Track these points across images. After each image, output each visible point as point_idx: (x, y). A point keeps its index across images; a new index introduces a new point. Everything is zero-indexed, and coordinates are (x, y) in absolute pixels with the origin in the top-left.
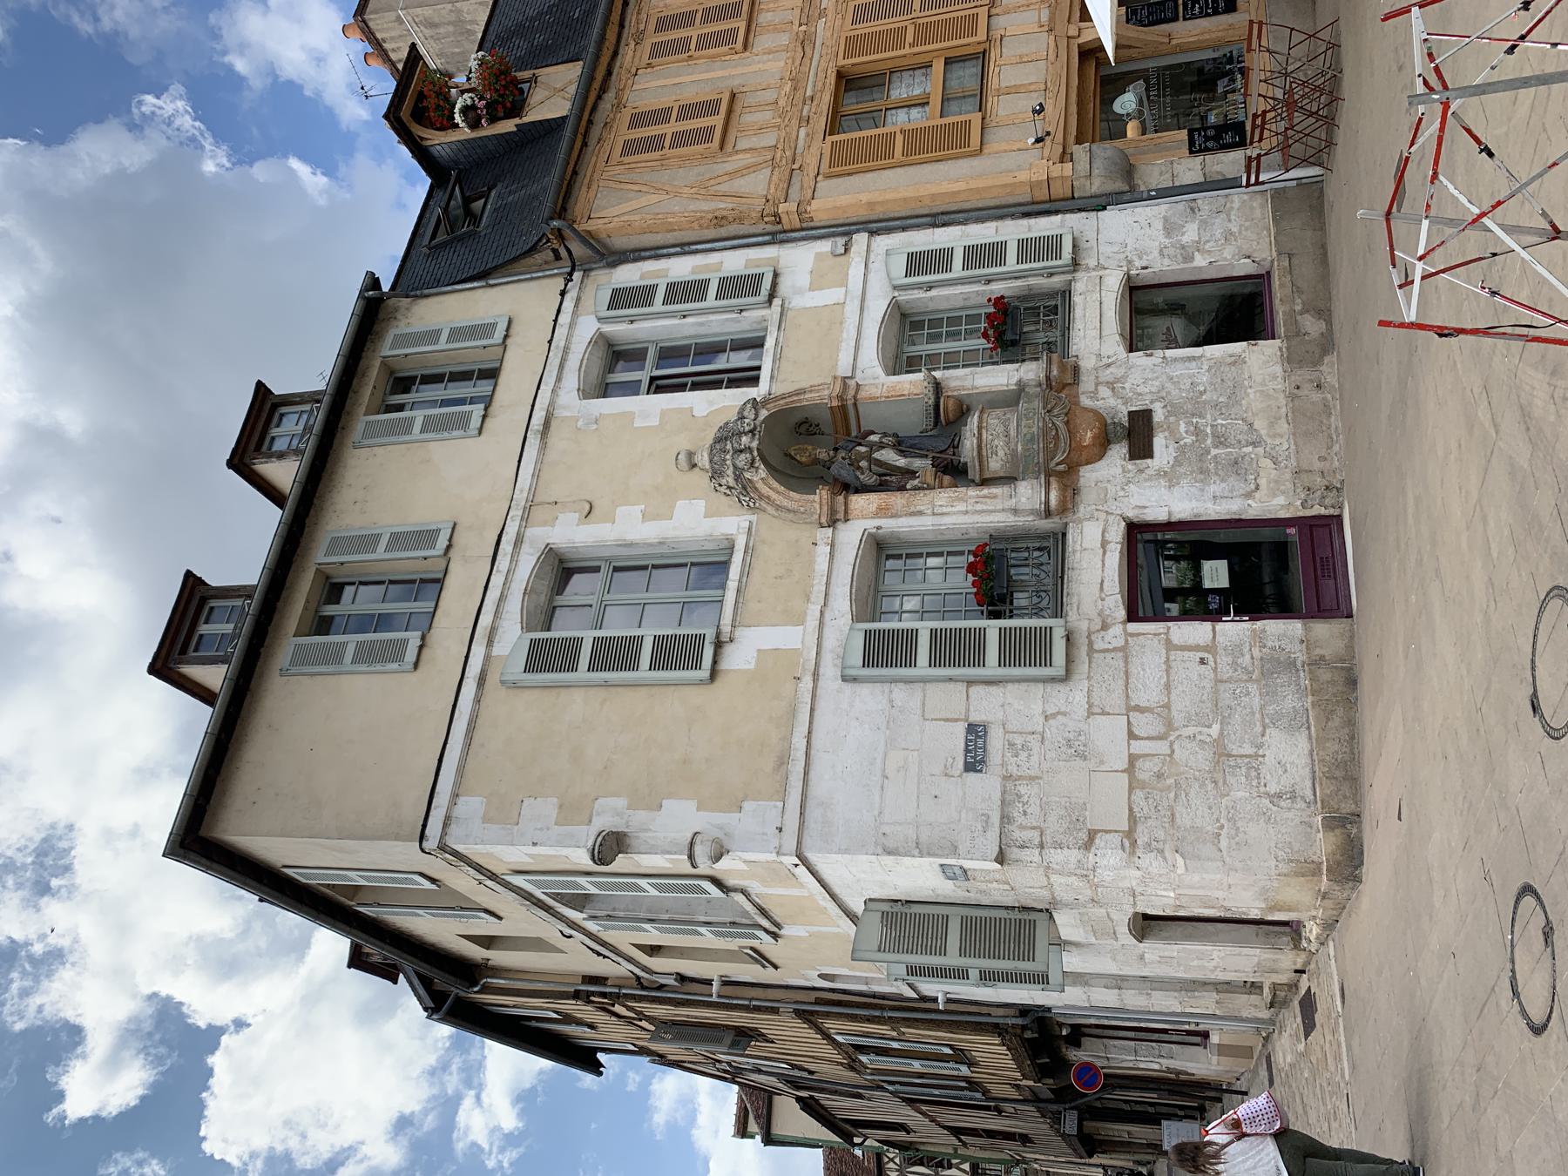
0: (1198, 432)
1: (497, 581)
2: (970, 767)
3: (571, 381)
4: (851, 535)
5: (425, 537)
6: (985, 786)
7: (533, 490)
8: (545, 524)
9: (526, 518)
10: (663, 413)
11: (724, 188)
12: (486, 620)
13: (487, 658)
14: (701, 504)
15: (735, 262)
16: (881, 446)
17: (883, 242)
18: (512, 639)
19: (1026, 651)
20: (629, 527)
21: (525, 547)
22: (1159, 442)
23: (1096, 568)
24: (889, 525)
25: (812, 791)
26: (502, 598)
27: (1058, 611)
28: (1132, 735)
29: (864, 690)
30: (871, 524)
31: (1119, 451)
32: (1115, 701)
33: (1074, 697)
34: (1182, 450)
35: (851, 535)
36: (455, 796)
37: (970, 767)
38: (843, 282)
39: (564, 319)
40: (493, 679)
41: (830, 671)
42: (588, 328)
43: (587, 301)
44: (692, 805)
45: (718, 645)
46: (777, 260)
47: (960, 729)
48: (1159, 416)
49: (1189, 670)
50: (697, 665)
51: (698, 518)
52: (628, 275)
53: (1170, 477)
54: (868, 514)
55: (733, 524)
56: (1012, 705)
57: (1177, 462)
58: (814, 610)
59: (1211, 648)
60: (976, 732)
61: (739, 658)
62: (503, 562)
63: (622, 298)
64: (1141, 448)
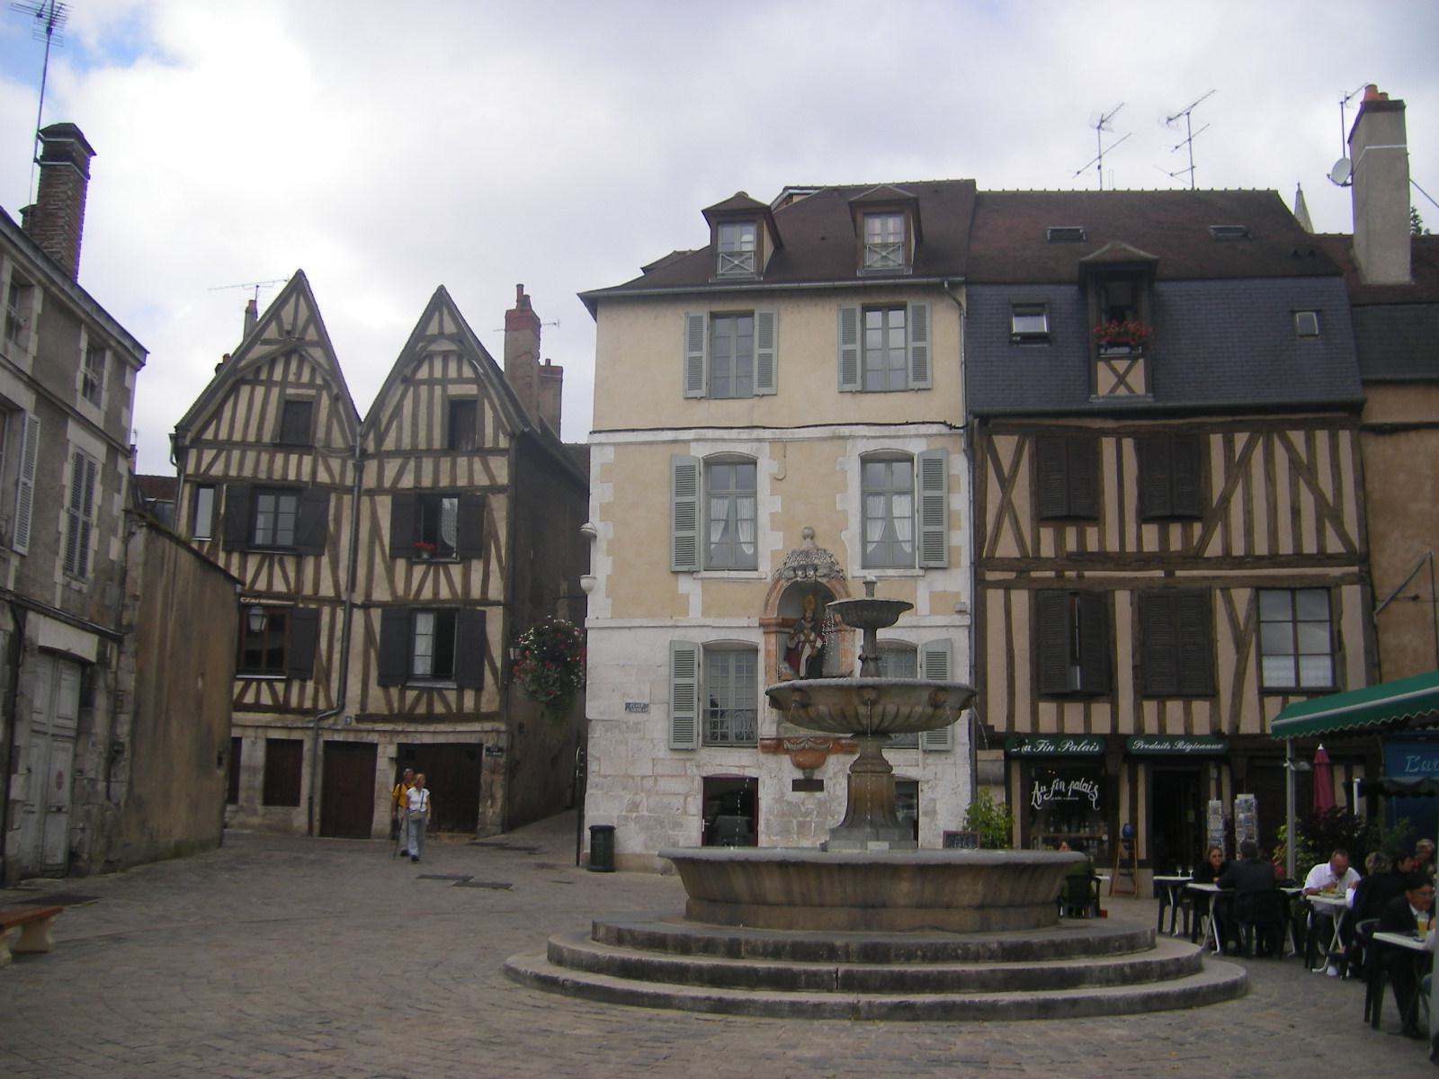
0: (807, 813)
1: (734, 434)
2: (628, 705)
3: (872, 446)
4: (757, 638)
5: (766, 378)
6: (620, 713)
7: (793, 441)
8: (771, 453)
9: (772, 441)
10: (845, 512)
11: (1007, 525)
12: (710, 434)
13: (688, 441)
14: (780, 546)
15: (960, 538)
16: (813, 647)
17: (962, 642)
18: (700, 451)
19: (681, 731)
20: (769, 503)
21: (755, 445)
22: (802, 794)
23: (731, 762)
24: (761, 655)
25: (616, 633)
26: (724, 440)
27: (706, 744)
28: (643, 777)
29: (667, 652)
30: (762, 647)
31: (799, 775)
32: (659, 770)
33: (662, 751)
34: (797, 805)
35: (757, 638)
36: (614, 444)
37: (628, 705)
38: (933, 612)
39: (923, 429)
40: (678, 449)
41: (677, 635)
42: (916, 447)
43: (940, 443)
44: (610, 572)
45: (691, 573)
46: (958, 565)
47: (646, 701)
48: (818, 795)
49: (677, 802)
50: (678, 562)
51: (772, 549)
52: (959, 466)
53: (780, 799)
54: (767, 645)
55: (766, 569)
56: (658, 724)
57: (789, 803)
58: (710, 621)
59: (685, 812)
60: (644, 708)
61: (686, 586)
62: (745, 434)
63: (934, 470)
64: (797, 785)
